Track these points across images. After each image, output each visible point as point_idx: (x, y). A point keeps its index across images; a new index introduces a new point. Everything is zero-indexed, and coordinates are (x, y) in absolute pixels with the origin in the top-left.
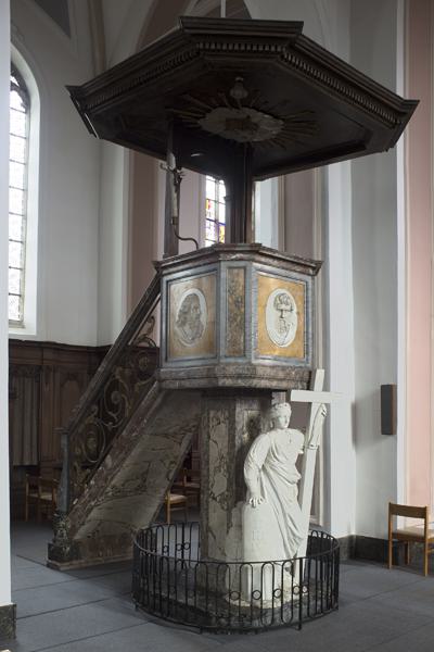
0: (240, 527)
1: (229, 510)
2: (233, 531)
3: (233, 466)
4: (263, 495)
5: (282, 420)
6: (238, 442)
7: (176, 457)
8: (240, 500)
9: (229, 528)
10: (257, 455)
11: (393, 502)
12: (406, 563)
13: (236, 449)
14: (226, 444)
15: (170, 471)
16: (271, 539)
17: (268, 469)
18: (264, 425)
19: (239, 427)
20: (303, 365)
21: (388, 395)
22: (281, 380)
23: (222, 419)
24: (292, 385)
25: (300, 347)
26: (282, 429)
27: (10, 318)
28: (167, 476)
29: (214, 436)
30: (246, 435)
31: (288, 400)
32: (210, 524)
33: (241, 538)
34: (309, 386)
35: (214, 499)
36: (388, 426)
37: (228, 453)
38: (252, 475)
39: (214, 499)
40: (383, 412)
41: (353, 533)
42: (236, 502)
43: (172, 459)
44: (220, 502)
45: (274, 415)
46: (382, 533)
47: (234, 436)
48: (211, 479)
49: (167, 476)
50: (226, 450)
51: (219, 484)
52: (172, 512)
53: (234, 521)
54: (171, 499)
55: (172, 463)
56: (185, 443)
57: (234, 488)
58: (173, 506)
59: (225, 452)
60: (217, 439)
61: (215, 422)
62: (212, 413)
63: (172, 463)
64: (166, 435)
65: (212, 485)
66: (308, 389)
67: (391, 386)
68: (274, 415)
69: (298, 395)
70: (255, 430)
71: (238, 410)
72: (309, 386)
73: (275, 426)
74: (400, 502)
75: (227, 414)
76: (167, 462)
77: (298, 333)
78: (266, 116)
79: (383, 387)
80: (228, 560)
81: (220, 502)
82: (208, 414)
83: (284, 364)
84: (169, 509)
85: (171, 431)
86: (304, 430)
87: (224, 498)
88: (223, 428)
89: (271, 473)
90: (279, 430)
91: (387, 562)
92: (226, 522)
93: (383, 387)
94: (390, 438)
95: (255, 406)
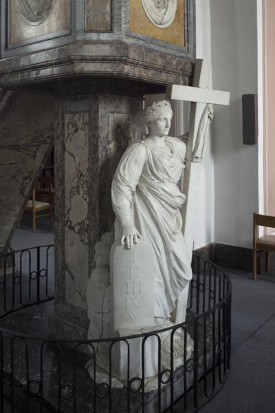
0: (107, 267)
1: (91, 245)
2: (96, 274)
3: (96, 186)
4: (139, 229)
5: (162, 124)
6: (101, 154)
7: (31, 172)
8: (105, 232)
9: (91, 268)
10: (130, 171)
11: (256, 213)
12: (267, 270)
13: (100, 163)
14: (86, 157)
15: (24, 188)
16: (150, 288)
17: (145, 191)
18: (134, 132)
19: (103, 134)
20: (183, 55)
21: (249, 104)
22: (160, 70)
23: (80, 125)
24: (172, 78)
25: (179, 32)
26: (161, 136)
27: (269, 253)
28: (22, 193)
29: (70, 146)
30: (112, 146)
31: (168, 98)
32: (68, 260)
33: (108, 282)
34: (192, 81)
35: (72, 228)
36: (250, 137)
37: (89, 169)
38: (124, 201)
39: (72, 228)
40: (242, 123)
41: (213, 241)
42: (100, 235)
43: (26, 175)
44: (79, 232)
45: (151, 118)
46: (244, 241)
47: (97, 146)
48: (67, 202)
49: (22, 193)
50: (87, 165)
51: (78, 209)
52: (36, 219)
53: (98, 260)
54: (36, 207)
55: (26, 178)
56: (40, 156)
57: (97, 215)
58: (39, 212)
59: (84, 168)
60: (74, 152)
61: (72, 129)
62: (67, 117)
63: (26, 178)
64: (16, 148)
65: (69, 210)
66: (191, 85)
67: (253, 95)
68: (151, 118)
69: (180, 92)
70: (123, 141)
71: (101, 112)
72: (192, 81)
73: (150, 132)
74: (261, 212)
75: (87, 118)
76: (20, 178)
77: (177, 13)
78: (44, 368)
79: (243, 96)
80: (89, 338)
81: (79, 232)
82: (63, 119)
83: (164, 50)
84: (34, 217)
85: (22, 142)
86: (186, 138)
87: (84, 228)
88: (83, 135)
89: (151, 198)
90: (158, 139)
91: (251, 270)
92: (87, 260)
93: (243, 96)
94: (251, 148)
95: (124, 108)
